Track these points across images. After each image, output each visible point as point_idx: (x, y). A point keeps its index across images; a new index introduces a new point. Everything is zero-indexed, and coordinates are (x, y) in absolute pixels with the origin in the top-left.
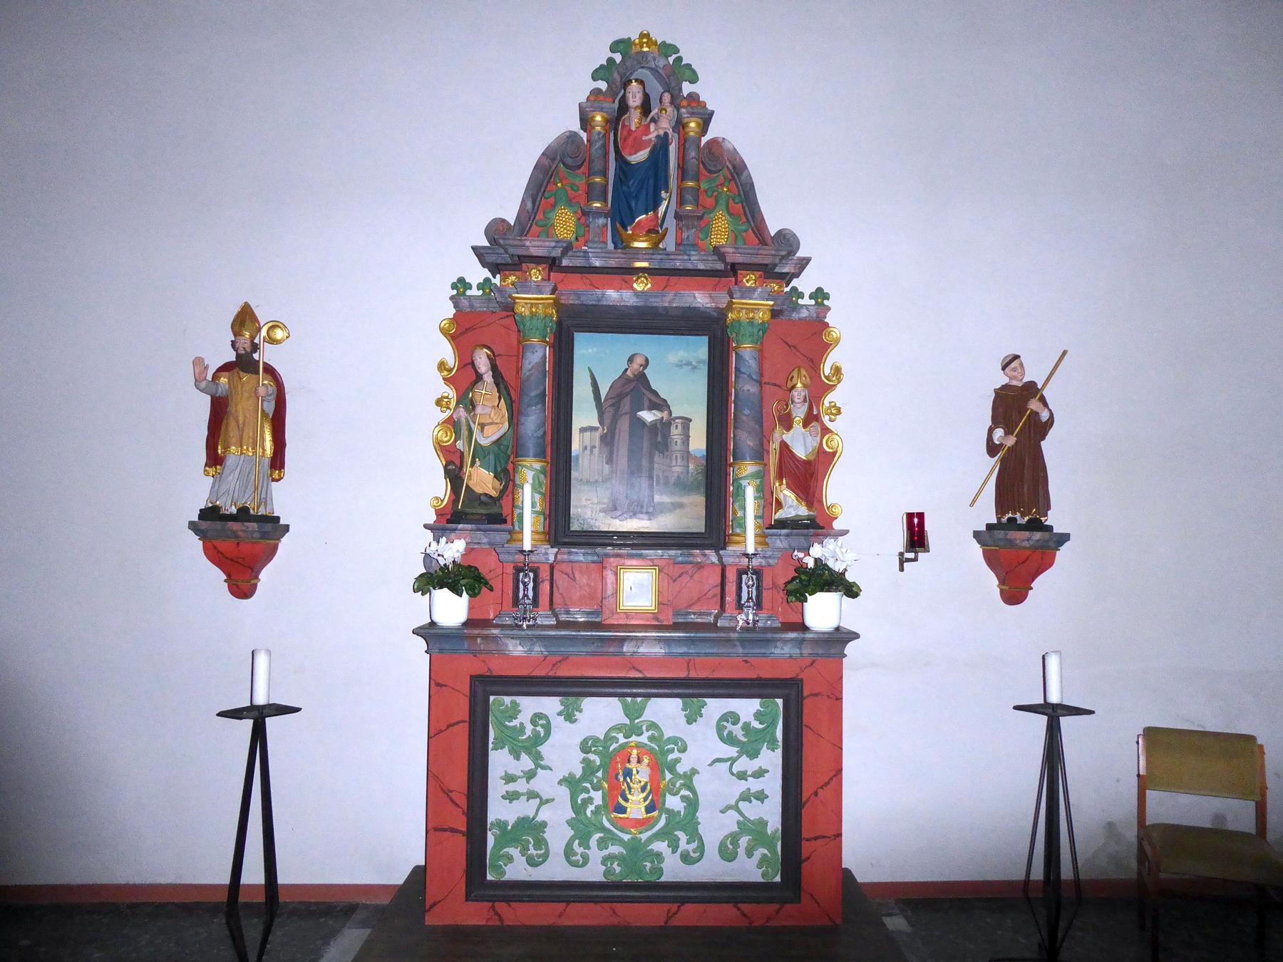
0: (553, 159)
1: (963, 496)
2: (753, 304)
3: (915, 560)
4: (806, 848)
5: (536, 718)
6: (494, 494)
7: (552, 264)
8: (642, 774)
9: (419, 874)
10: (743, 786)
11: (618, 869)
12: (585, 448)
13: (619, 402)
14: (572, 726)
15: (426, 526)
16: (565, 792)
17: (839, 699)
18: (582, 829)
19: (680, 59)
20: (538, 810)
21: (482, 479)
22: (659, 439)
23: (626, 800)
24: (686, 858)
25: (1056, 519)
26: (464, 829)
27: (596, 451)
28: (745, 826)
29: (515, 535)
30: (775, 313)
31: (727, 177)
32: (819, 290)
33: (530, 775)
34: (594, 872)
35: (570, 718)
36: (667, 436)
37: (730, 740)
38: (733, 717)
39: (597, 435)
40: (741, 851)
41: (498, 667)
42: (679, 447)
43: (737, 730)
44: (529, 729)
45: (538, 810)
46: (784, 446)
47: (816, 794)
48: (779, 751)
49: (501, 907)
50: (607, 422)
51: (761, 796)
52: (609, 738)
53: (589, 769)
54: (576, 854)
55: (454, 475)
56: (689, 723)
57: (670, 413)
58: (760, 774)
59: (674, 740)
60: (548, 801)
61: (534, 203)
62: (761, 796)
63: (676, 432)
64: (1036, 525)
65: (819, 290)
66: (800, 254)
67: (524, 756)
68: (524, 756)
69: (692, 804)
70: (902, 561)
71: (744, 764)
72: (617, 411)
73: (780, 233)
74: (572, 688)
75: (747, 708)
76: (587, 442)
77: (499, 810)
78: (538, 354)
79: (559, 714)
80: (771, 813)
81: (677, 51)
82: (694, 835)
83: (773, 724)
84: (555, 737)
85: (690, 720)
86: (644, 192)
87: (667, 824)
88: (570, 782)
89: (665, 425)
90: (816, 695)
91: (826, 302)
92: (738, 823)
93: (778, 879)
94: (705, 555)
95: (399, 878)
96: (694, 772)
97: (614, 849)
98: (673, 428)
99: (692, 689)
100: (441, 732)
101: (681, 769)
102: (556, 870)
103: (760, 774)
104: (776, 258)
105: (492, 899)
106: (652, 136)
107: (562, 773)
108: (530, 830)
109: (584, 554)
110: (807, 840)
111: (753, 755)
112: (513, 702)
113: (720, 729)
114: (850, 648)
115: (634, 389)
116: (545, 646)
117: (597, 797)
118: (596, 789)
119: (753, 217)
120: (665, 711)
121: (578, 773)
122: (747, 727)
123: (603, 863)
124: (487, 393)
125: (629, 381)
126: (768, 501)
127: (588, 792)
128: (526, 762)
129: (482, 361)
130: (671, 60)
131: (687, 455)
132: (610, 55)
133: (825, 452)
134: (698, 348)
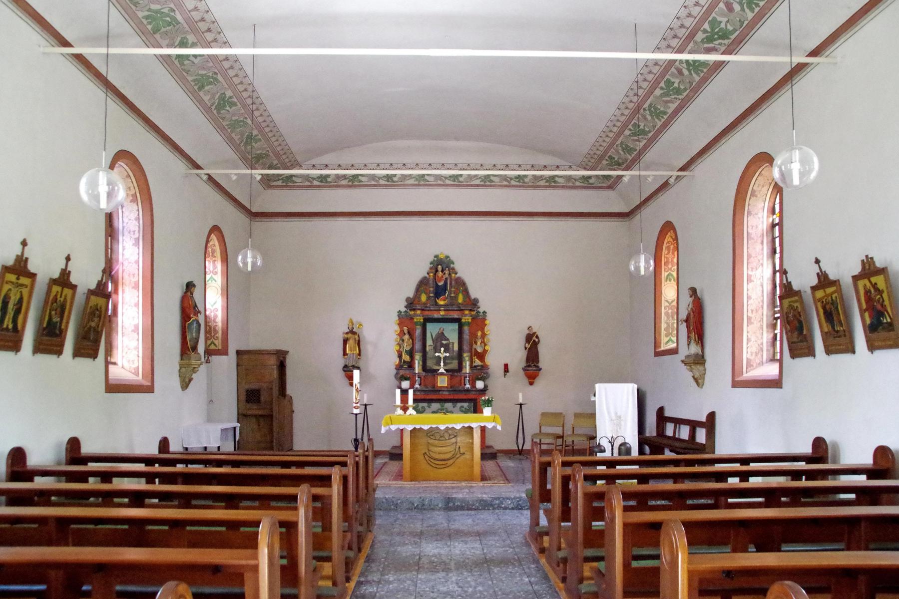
1: (517, 357)
2: (467, 319)
21: (406, 358)
25: (541, 365)
29: (414, 369)
31: (461, 284)
38: (462, 407)
55: (400, 356)
56: (441, 264)
75: (466, 405)
78: (418, 331)
99: (455, 401)
104: (473, 304)
124: (407, 337)
129: (405, 328)
134: (456, 326)
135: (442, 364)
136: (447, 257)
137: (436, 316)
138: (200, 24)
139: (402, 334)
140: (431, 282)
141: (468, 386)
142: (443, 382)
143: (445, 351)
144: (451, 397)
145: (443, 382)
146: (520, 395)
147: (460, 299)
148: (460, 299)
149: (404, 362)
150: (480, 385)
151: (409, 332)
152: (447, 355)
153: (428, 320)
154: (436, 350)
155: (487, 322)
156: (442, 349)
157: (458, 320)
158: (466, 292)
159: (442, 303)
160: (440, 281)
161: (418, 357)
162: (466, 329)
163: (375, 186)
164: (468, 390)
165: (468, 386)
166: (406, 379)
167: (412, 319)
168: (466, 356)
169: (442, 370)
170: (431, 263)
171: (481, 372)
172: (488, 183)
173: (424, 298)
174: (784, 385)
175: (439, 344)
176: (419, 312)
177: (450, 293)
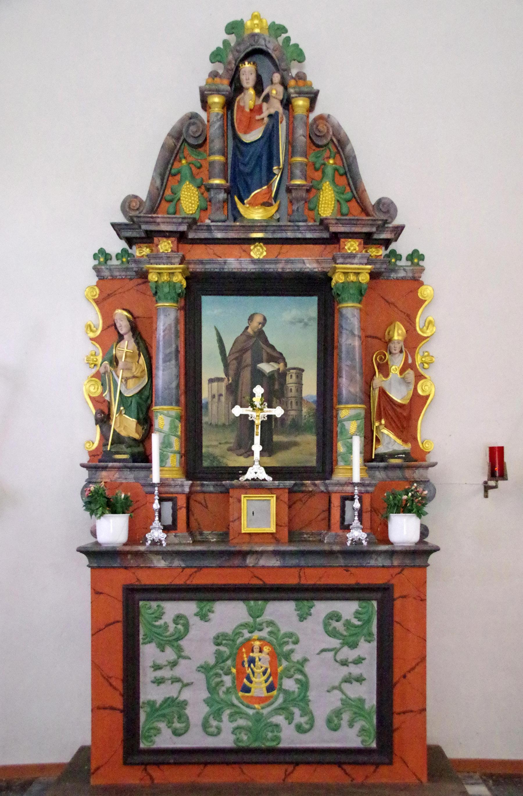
0: (178, 139)
2: (351, 268)
3: (496, 487)
4: (397, 720)
5: (178, 618)
6: (137, 436)
7: (181, 238)
8: (263, 659)
9: (83, 752)
10: (344, 671)
11: (245, 738)
12: (214, 396)
13: (241, 356)
14: (207, 624)
15: (83, 466)
16: (201, 677)
17: (423, 600)
18: (216, 707)
19: (288, 39)
20: (180, 692)
21: (127, 426)
23: (251, 682)
24: (299, 728)
26: (121, 707)
27: (223, 399)
28: (346, 702)
30: (374, 275)
31: (330, 145)
32: (416, 251)
33: (174, 664)
34: (225, 740)
35: (204, 617)
36: (283, 384)
37: (333, 634)
38: (336, 616)
39: (223, 385)
40: (344, 723)
41: (146, 579)
42: (293, 393)
43: (339, 626)
44: (172, 627)
45: (180, 692)
46: (383, 392)
47: (404, 677)
48: (375, 644)
49: (153, 771)
50: (231, 372)
51: (360, 679)
52: (237, 634)
53: (220, 658)
54: (211, 727)
55: (103, 419)
57: (286, 365)
58: (358, 661)
59: (291, 635)
60: (187, 685)
61: (162, 180)
62: (360, 679)
63: (291, 381)
65: (416, 251)
66: (397, 222)
69: (304, 685)
70: (487, 488)
71: (347, 653)
72: (239, 363)
73: (379, 201)
75: (348, 609)
76: (215, 392)
77: (150, 693)
78: (166, 320)
79: (196, 615)
80: (367, 693)
81: (286, 31)
82: (306, 712)
83: (368, 621)
84: (193, 633)
85: (302, 618)
86: (258, 169)
87: (285, 701)
88: (205, 669)
89: (282, 375)
90: (404, 597)
91: (421, 263)
92: (342, 700)
93: (374, 745)
94: (315, 485)
95: (65, 756)
96: (306, 660)
97: (241, 722)
98: (288, 378)
101: (296, 657)
102: (194, 739)
103: (358, 661)
104: (377, 226)
105: (146, 764)
106: (265, 114)
108: (174, 709)
109: (214, 486)
110: (399, 714)
111: (353, 646)
112: (158, 606)
113: (326, 625)
115: (255, 345)
116: (183, 560)
117: (228, 680)
118: (226, 674)
119: (356, 188)
121: (212, 661)
122: (348, 624)
123: (233, 733)
124: (127, 347)
125: (249, 337)
126: (369, 438)
127: (220, 676)
128: (170, 654)
129: (121, 317)
130: (281, 39)
131: (300, 400)
132: (226, 37)
133: (419, 396)
134: (308, 307)
135: (257, 448)
136: (278, 30)
137: (234, 262)
139: (110, 334)
140: (215, 130)
141: (357, 533)
142: (258, 515)
143: (270, 400)
144: (291, 579)
145: (258, 515)
147: (327, 203)
148: (327, 203)
149: (118, 439)
150: (403, 529)
151: (134, 329)
152: (278, 412)
153: (201, 285)
154: (236, 394)
155: (425, 292)
156: (259, 390)
157: (314, 285)
158: (349, 175)
159: (256, 214)
160: (248, 129)
161: (166, 420)
162: (350, 312)
164: (357, 552)
165: (357, 533)
166: (113, 507)
167: (143, 275)
168: (349, 417)
169: (257, 472)
170: (216, 56)
171: (404, 482)
173: (189, 199)
174: (488, 450)
175: (246, 374)
176: (165, 246)
177: (289, 171)
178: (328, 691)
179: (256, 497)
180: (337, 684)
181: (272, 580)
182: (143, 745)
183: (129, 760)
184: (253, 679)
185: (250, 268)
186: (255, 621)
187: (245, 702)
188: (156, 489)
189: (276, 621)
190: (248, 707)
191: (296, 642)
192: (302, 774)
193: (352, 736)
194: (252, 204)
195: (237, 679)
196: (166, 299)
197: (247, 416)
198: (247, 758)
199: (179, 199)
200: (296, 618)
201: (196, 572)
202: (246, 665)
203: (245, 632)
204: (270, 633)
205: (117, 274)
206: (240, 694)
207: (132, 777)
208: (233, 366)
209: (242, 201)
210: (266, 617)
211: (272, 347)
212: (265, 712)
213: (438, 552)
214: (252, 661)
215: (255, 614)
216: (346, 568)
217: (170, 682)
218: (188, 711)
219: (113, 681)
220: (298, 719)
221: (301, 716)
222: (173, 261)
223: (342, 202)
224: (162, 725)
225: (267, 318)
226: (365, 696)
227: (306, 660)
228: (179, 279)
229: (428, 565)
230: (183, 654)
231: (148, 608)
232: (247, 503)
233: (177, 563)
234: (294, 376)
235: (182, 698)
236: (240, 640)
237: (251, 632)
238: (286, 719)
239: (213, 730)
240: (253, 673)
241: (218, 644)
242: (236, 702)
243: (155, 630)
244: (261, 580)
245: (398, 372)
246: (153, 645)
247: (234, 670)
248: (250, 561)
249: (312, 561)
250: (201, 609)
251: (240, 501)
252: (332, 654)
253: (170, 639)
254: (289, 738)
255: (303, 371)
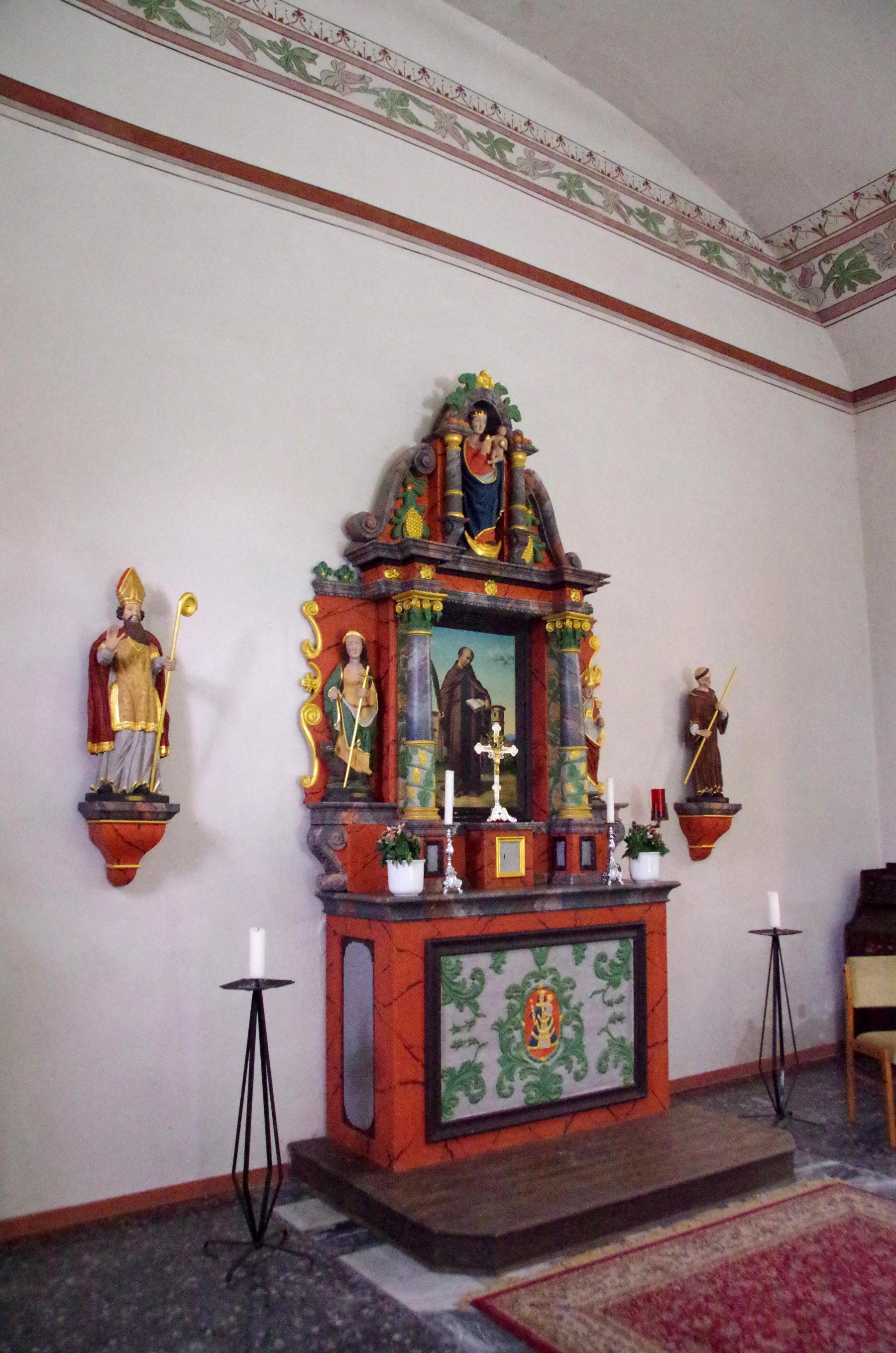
8: (547, 1006)
10: (610, 1012)
16: (495, 1034)
17: (665, 934)
18: (508, 1062)
22: (483, 725)
23: (537, 1033)
24: (578, 1077)
28: (612, 1042)
33: (471, 1024)
34: (516, 1101)
38: (602, 957)
40: (610, 1064)
41: (447, 930)
43: (604, 965)
44: (469, 982)
48: (632, 981)
50: (444, 707)
52: (526, 983)
57: (490, 702)
59: (569, 980)
60: (483, 1045)
64: (718, 797)
67: (466, 1008)
68: (466, 1008)
69: (579, 1030)
74: (498, 943)
75: (611, 948)
77: (451, 1060)
80: (626, 1031)
82: (582, 1059)
84: (488, 988)
88: (499, 1026)
92: (608, 1041)
93: (632, 1082)
97: (531, 1078)
98: (492, 715)
99: (577, 936)
100: (402, 994)
101: (574, 1003)
102: (492, 1104)
107: (492, 1020)
110: (414, 1082)
112: (458, 961)
114: (672, 895)
115: (463, 680)
117: (517, 1034)
120: (560, 956)
121: (505, 1017)
122: (613, 965)
124: (355, 673)
138: (538, 522)
144: (566, 922)
146: (257, 939)
158: (546, 529)
163: (237, 63)
172: (576, 200)
178: (599, 1034)
179: (510, 838)
180: (604, 1026)
181: (555, 924)
182: (446, 1118)
183: (434, 1138)
184: (540, 1031)
185: (485, 603)
186: (540, 969)
187: (534, 1057)
188: (449, 831)
189: (558, 969)
190: (535, 1061)
191: (572, 988)
192: (581, 1124)
193: (617, 1077)
194: (480, 541)
195: (526, 1032)
196: (419, 627)
197: (487, 753)
198: (536, 1115)
199: (404, 524)
200: (571, 963)
201: (490, 921)
202: (534, 1017)
203: (532, 981)
204: (554, 979)
205: (340, 591)
206: (529, 1048)
207: (433, 1157)
208: (445, 701)
209: (473, 537)
210: (550, 963)
211: (479, 683)
212: (548, 1064)
213: (678, 888)
214: (539, 1011)
215: (539, 962)
216: (610, 908)
217: (467, 1044)
218: (484, 1075)
219: (414, 1051)
220: (577, 1067)
221: (579, 1063)
222: (435, 589)
223: (538, 550)
224: (460, 1094)
225: (475, 656)
226: (625, 1035)
227: (581, 1004)
228: (439, 607)
229: (668, 901)
230: (479, 1012)
231: (449, 962)
232: (500, 845)
233: (476, 912)
234: (497, 714)
235: (478, 1061)
236: (528, 991)
237: (536, 981)
238: (567, 1068)
239: (506, 1091)
240: (540, 1023)
241: (509, 997)
242: (526, 1058)
243: (454, 987)
244: (544, 924)
245: (591, 715)
246: (453, 1005)
247: (523, 1024)
248: (537, 906)
249: (587, 902)
250: (495, 960)
251: (494, 844)
252: (600, 995)
253: (468, 996)
254: (571, 1088)
255: (504, 709)
